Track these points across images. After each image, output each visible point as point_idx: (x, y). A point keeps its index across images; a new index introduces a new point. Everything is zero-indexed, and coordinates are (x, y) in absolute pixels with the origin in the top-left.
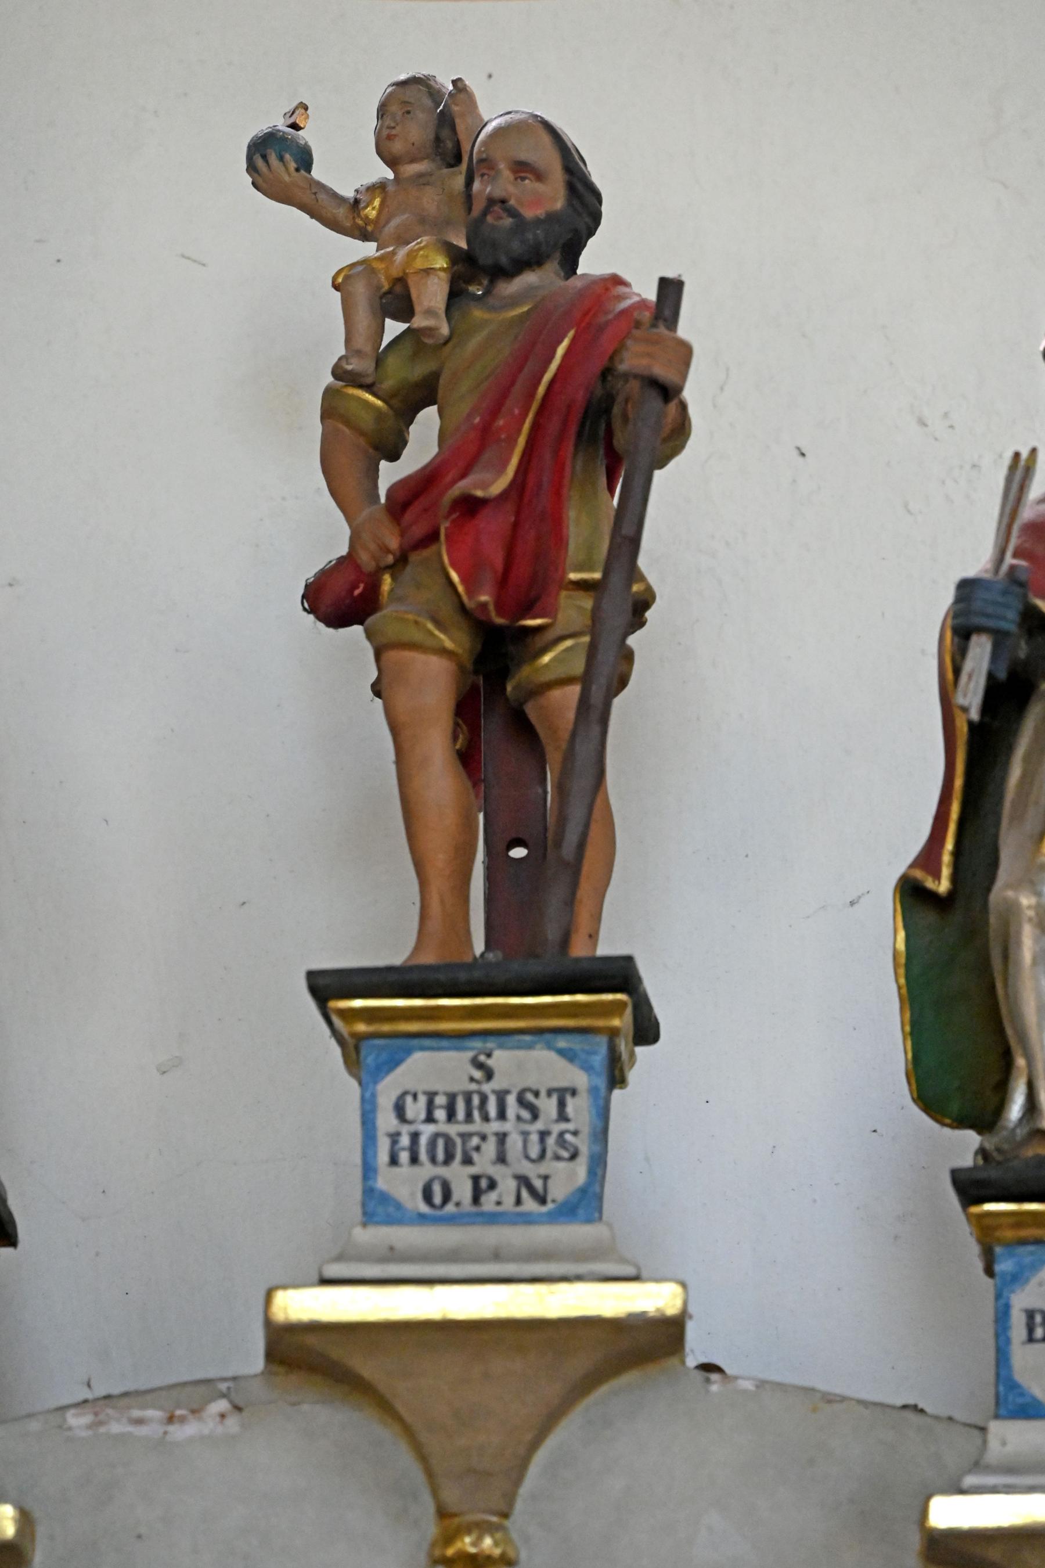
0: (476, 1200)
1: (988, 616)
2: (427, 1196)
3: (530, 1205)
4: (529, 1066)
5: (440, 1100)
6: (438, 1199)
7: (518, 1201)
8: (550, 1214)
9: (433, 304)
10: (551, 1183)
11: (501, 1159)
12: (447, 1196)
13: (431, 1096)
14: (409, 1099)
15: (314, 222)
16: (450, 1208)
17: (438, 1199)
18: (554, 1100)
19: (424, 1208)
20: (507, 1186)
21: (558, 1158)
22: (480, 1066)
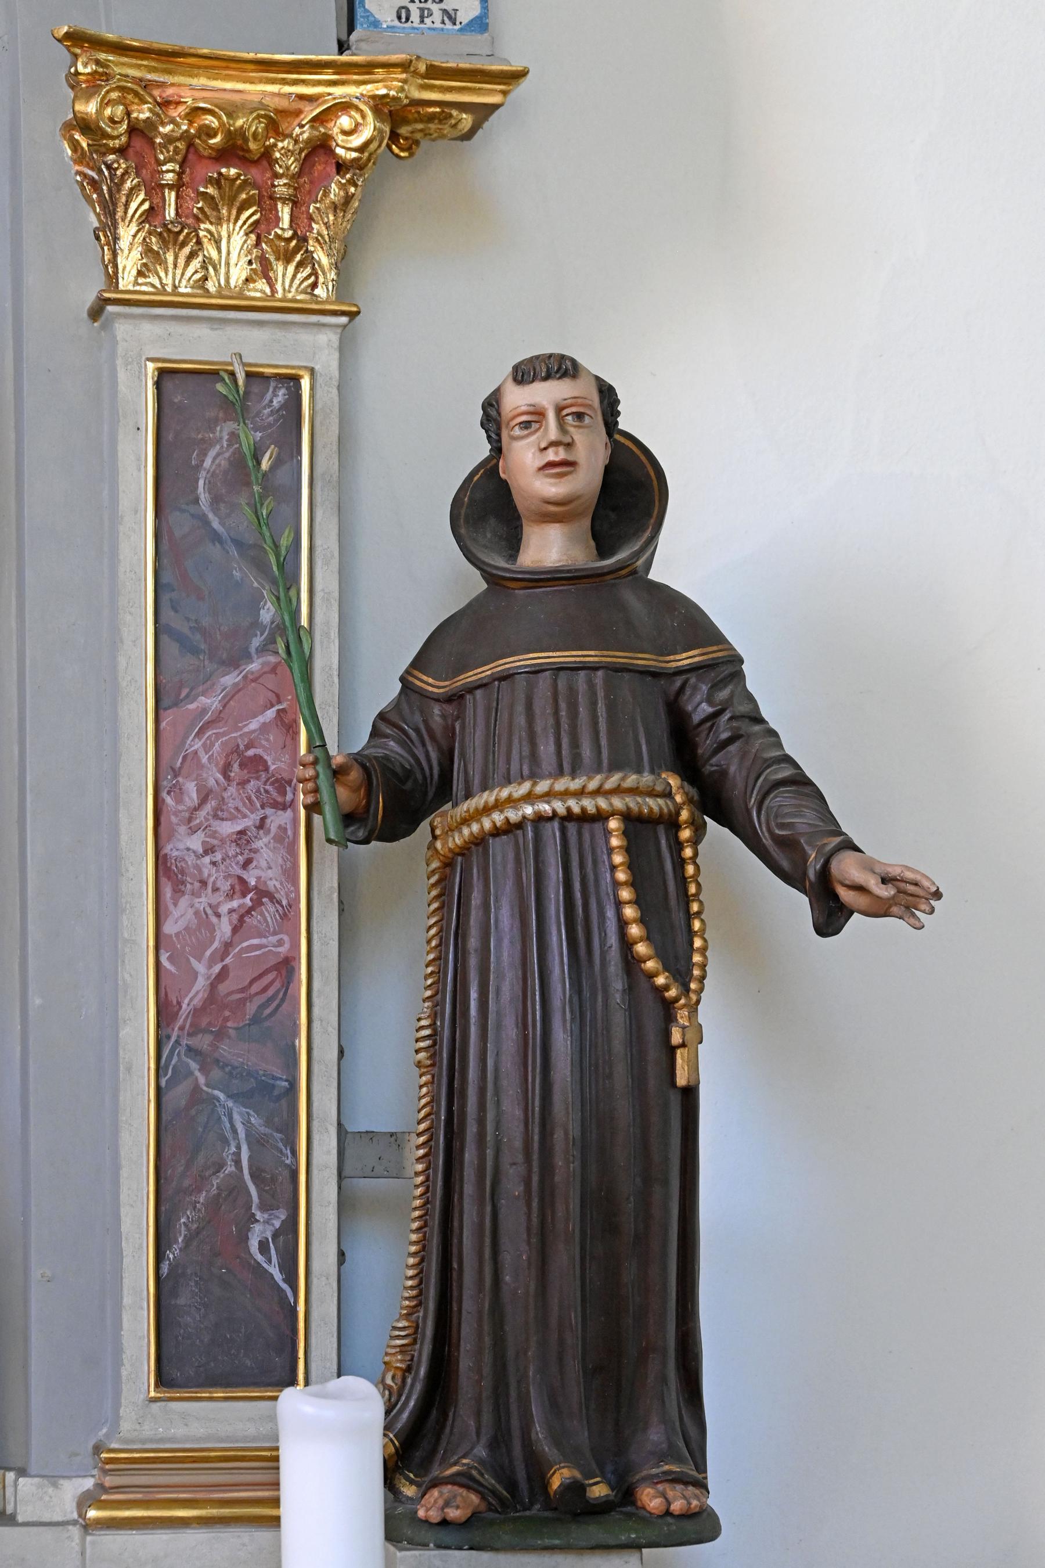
0: (422, 22)
2: (399, 18)
3: (449, 26)
6: (403, 20)
7: (443, 22)
10: (458, 13)
12: (407, 19)
16: (409, 24)
17: (403, 20)
19: (396, 23)
20: (437, 16)
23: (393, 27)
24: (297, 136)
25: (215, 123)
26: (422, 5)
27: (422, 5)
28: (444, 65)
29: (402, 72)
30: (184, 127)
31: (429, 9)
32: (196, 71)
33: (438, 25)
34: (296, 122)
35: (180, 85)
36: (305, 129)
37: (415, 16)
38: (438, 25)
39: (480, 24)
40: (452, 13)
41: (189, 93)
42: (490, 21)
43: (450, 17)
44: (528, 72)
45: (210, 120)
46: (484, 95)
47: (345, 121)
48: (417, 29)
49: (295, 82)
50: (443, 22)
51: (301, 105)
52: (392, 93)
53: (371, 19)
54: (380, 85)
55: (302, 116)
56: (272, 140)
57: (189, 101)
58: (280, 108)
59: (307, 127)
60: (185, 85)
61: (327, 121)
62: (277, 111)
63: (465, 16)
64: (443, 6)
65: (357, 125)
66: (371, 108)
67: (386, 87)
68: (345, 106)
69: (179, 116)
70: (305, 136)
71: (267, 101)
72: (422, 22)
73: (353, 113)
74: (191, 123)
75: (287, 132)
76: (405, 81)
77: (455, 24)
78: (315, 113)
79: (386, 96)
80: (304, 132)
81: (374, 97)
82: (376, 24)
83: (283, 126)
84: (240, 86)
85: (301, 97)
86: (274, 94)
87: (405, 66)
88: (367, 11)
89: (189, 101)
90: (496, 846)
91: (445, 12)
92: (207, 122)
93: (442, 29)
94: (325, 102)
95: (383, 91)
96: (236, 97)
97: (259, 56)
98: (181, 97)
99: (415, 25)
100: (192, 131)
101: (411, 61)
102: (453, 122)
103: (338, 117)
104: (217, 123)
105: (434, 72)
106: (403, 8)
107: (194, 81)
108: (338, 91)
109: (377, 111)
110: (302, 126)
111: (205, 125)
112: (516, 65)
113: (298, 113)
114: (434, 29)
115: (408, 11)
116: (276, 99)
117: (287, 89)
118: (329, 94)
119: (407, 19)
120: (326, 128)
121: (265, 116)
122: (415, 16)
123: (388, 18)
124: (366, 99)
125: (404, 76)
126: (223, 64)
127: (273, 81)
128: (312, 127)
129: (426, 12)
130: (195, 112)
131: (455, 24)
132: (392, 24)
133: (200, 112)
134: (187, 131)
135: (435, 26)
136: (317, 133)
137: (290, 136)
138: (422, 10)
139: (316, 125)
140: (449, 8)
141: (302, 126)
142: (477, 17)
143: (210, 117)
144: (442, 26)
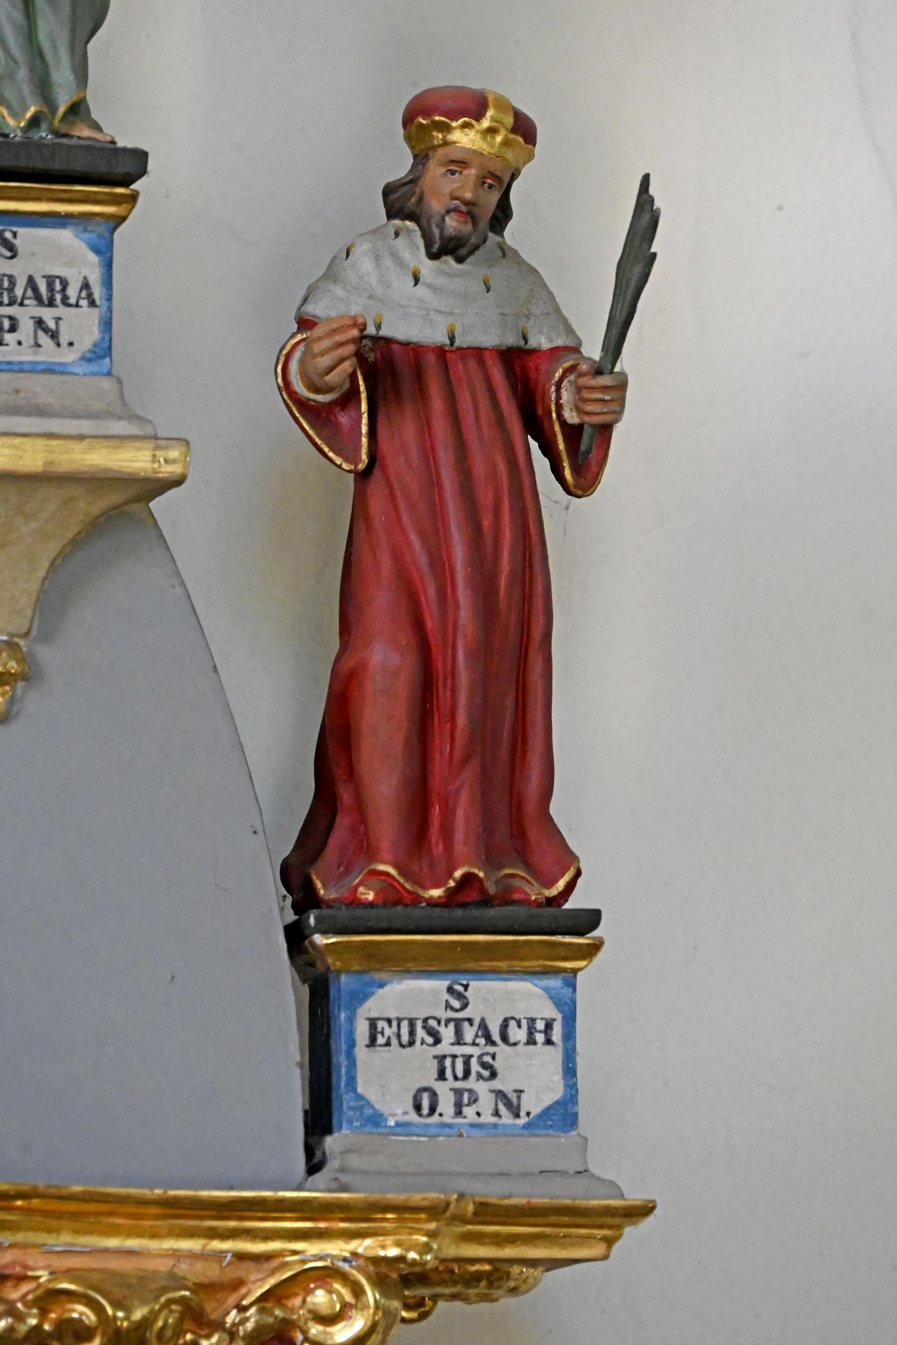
0: (459, 1113)
1: (427, 600)
2: (418, 1108)
3: (507, 1118)
4: (501, 997)
5: (540, 1025)
6: (425, 1111)
7: (497, 1114)
8: (527, 1126)
9: (79, 447)
10: (524, 1096)
11: (441, 1076)
12: (432, 1110)
13: (532, 1021)
14: (513, 1024)
15: (534, 465)
16: (435, 1118)
17: (425, 1111)
18: (452, 1026)
19: (413, 1117)
20: (486, 1103)
21: (480, 1077)
22: (460, 996)
23: (407, 1124)
24: (234, 1324)
25: (90, 1317)
26: (459, 1085)
27: (459, 1085)
28: (506, 1202)
29: (429, 1221)
30: (33, 1322)
31: (470, 1091)
32: (55, 1223)
33: (488, 1118)
34: (232, 1300)
35: (24, 1246)
36: (248, 1314)
37: (446, 1105)
38: (488, 1118)
39: (563, 1115)
40: (513, 1097)
41: (42, 1261)
42: (583, 1108)
43: (509, 1104)
44: (653, 1209)
45: (79, 1311)
46: (572, 1245)
47: (320, 1298)
48: (449, 1126)
49: (233, 1234)
50: (497, 1114)
51: (244, 1270)
52: (412, 1255)
53: (368, 1112)
54: (389, 1240)
55: (243, 1291)
56: (189, 1337)
57: (44, 1276)
58: (204, 1280)
59: (253, 1310)
60: (35, 1246)
61: (288, 1297)
62: (199, 1288)
63: (534, 1103)
64: (496, 1084)
65: (345, 1306)
66: (369, 1278)
67: (398, 1244)
68: (326, 1275)
69: (23, 1298)
70: (250, 1326)
71: (183, 1268)
72: (459, 1113)
73: (337, 1286)
74: (43, 1313)
75: (214, 1316)
76: (433, 1235)
77: (517, 1116)
78: (266, 1287)
79: (401, 1259)
80: (247, 1319)
81: (377, 1261)
82: (376, 1119)
83: (211, 1310)
84: (132, 1243)
85: (241, 1257)
86: (192, 1256)
87: (435, 1211)
88: (360, 1097)
89: (44, 1276)
90: (322, 1186)
91: (500, 1094)
92: (75, 1315)
93: (495, 1126)
94: (285, 1265)
95: (393, 1252)
96: (127, 1265)
97: (172, 1193)
98: (26, 1267)
99: (447, 1119)
100: (47, 1327)
101: (448, 1205)
102: (512, 1284)
103: (311, 1292)
104: (93, 1318)
105: (487, 1212)
106: (425, 1089)
107: (50, 1240)
108: (312, 1248)
109: (379, 1282)
110: (242, 1309)
111: (72, 1320)
112: (634, 1196)
113: (238, 1284)
114: (479, 1126)
115: (434, 1095)
116: (199, 1266)
117: (217, 1245)
118: (295, 1252)
119: (432, 1110)
120: (283, 1306)
121: (181, 1301)
122: (446, 1105)
123: (397, 1109)
124: (361, 1262)
125: (433, 1226)
126: (104, 1207)
127: (192, 1234)
128: (261, 1311)
129: (466, 1097)
130: (50, 1298)
131: (517, 1116)
132: (406, 1118)
133: (63, 1298)
134: (38, 1328)
135: (482, 1120)
136: (270, 1320)
137: (219, 1326)
138: (458, 1093)
139: (268, 1305)
140: (507, 1088)
141: (242, 1309)
142: (557, 1102)
143: (80, 1308)
144: (495, 1120)
